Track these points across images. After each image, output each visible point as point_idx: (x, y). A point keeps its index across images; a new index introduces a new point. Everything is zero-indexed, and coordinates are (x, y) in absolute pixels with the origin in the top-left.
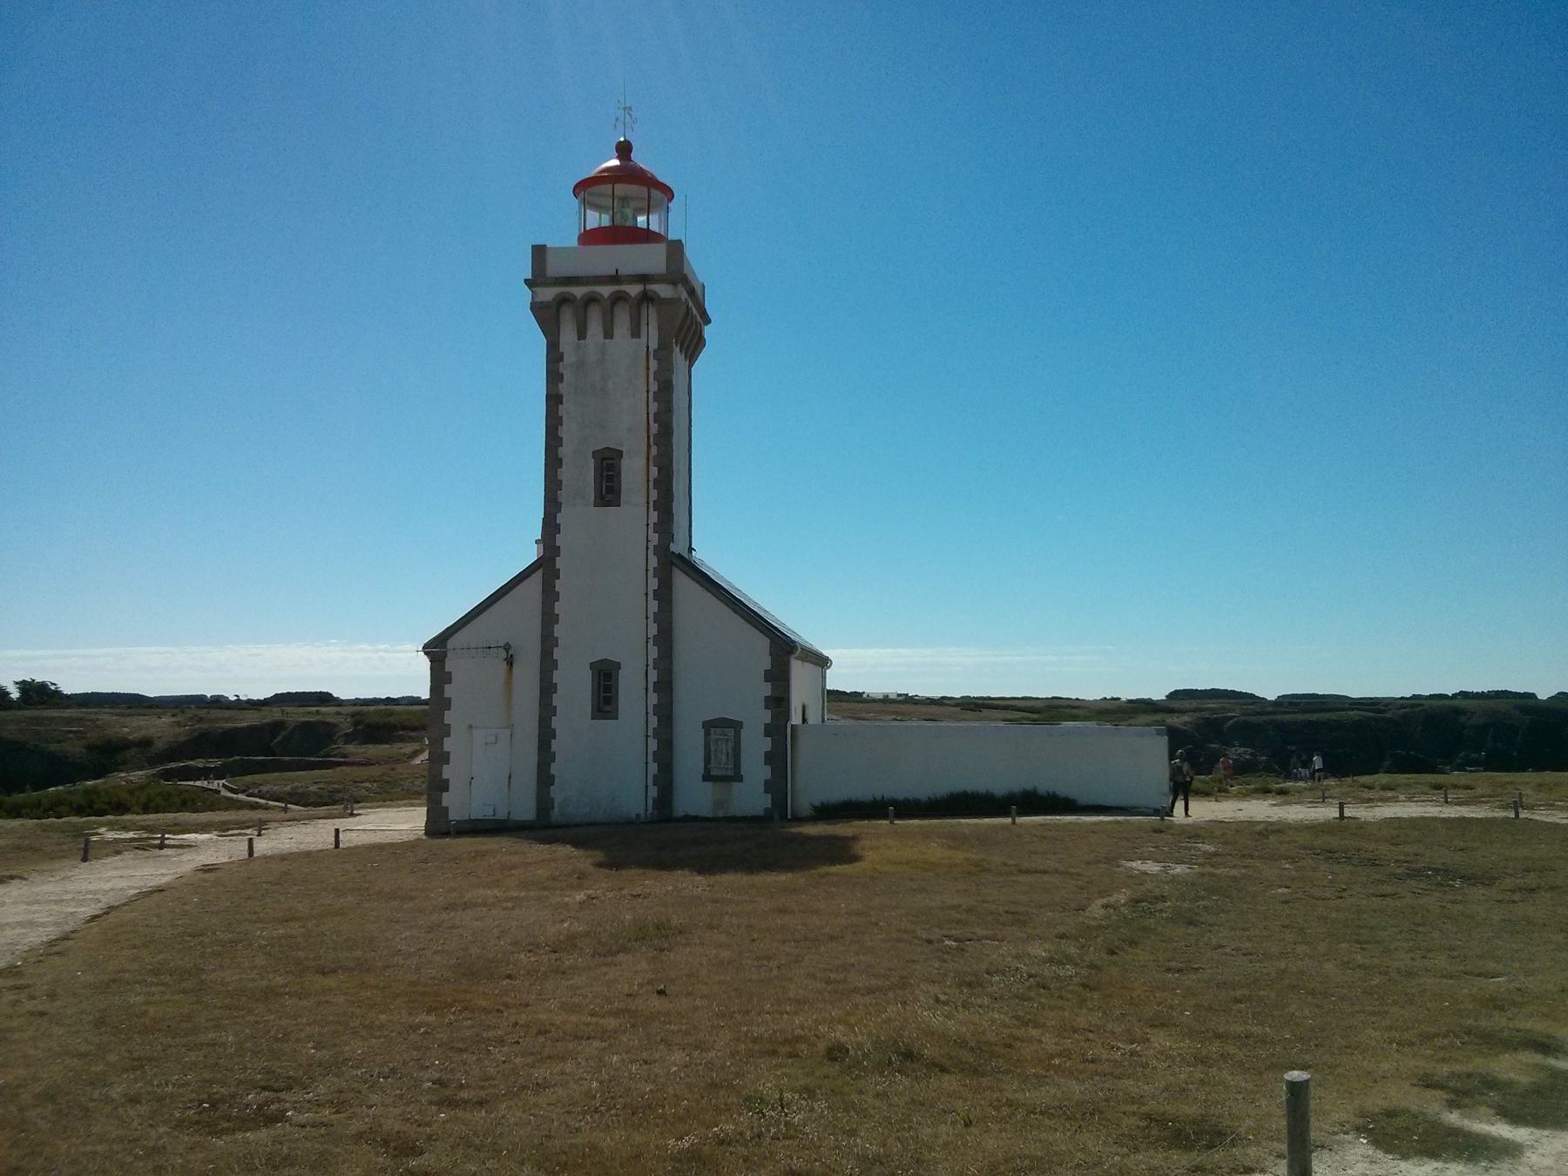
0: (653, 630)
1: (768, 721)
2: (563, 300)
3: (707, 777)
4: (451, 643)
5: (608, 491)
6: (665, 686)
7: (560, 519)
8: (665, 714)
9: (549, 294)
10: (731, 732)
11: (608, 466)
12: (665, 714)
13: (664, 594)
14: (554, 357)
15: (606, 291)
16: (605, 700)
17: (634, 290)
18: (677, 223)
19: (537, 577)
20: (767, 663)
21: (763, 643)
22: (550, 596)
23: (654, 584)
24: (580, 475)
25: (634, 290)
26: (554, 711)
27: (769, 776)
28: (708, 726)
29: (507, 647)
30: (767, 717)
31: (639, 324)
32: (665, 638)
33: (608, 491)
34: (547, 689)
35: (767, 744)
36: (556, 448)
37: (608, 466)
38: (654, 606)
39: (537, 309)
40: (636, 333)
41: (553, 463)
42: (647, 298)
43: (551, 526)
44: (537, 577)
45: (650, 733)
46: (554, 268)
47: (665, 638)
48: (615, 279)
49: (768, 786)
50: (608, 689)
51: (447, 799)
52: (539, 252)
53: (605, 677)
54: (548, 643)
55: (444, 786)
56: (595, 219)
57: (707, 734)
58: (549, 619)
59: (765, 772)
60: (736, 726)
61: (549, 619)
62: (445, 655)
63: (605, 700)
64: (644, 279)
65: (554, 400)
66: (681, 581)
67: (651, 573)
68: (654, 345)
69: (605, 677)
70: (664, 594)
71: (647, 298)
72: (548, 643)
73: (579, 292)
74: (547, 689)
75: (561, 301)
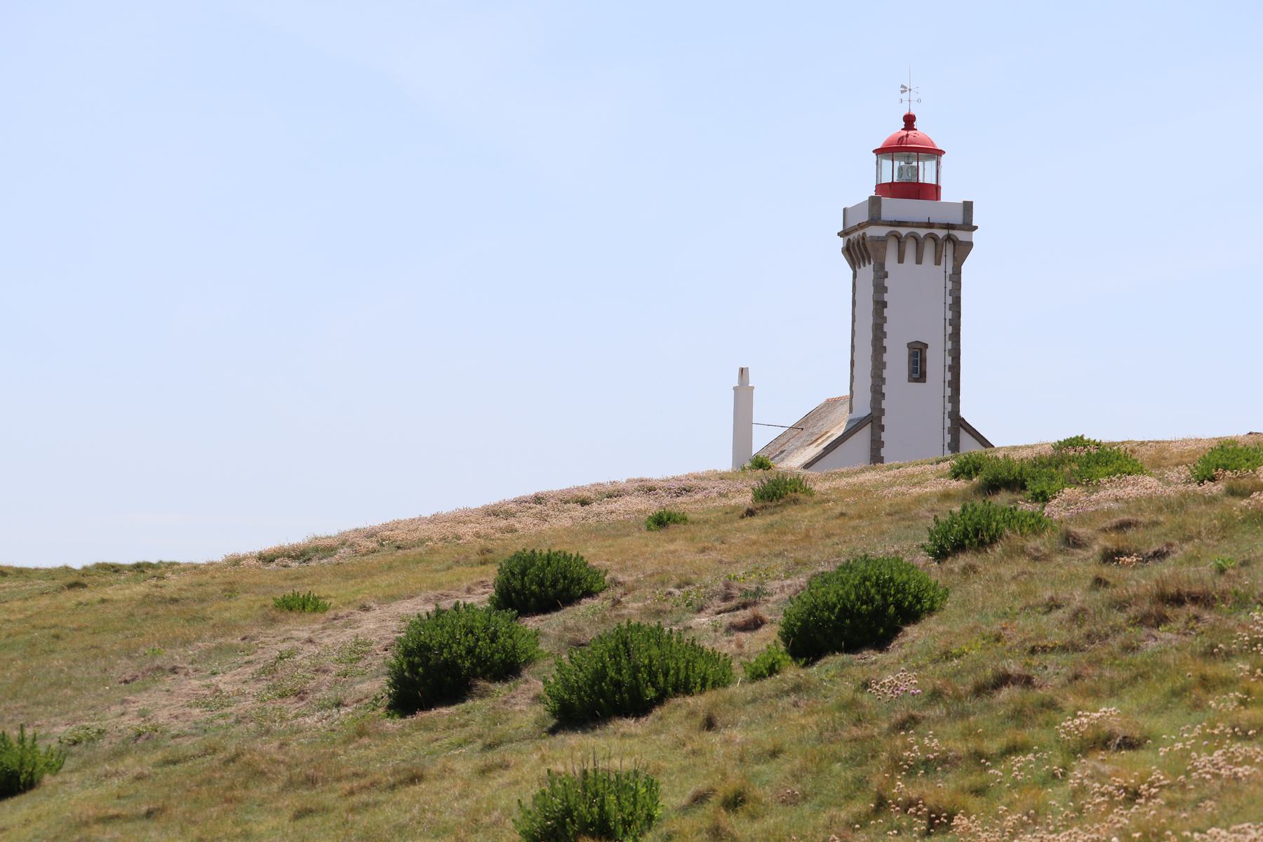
14: (855, 276)
23: (948, 438)
24: (936, 362)
25: (941, 233)
40: (938, 263)
42: (949, 238)
43: (877, 394)
48: (930, 225)
64: (949, 226)
66: (964, 435)
68: (950, 271)
71: (949, 238)
73: (904, 231)
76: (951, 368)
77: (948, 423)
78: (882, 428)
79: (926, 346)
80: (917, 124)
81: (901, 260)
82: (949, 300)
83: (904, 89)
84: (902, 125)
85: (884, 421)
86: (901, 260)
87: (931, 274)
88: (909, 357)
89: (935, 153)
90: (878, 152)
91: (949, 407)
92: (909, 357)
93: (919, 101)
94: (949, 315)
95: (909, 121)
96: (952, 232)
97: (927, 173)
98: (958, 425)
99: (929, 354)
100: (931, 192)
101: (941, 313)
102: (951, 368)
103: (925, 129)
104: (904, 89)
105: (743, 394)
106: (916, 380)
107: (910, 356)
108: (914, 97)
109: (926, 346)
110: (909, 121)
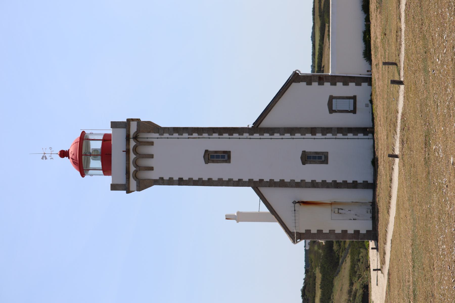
0: (288, 135)
1: (329, 83)
2: (135, 177)
3: (354, 111)
4: (292, 229)
5: (224, 157)
6: (313, 131)
7: (236, 179)
8: (325, 131)
9: (133, 183)
10: (334, 101)
11: (211, 157)
12: (325, 131)
13: (272, 131)
14: (161, 182)
15: (132, 156)
16: (321, 158)
17: (133, 143)
18: (99, 127)
19: (262, 190)
20: (304, 84)
21: (294, 85)
22: (272, 184)
23: (266, 135)
24: (217, 170)
25: (133, 143)
26: (271, 181)
27: (354, 84)
28: (331, 111)
29: (295, 203)
30: (327, 84)
31: (144, 142)
32: (292, 131)
33: (224, 157)
34: (314, 185)
35: (340, 84)
36: (203, 181)
37: (211, 157)
38: (277, 135)
39: (140, 188)
40: (152, 144)
41: (210, 183)
42: (136, 138)
43: (239, 183)
44: (262, 190)
45: (334, 137)
46: (122, 181)
47: (292, 131)
48: (127, 152)
49: (358, 84)
50: (315, 158)
51: (363, 231)
52: (114, 187)
53: (307, 158)
54: (294, 184)
55: (357, 232)
56: (96, 163)
57: (335, 111)
58: (282, 184)
59: (352, 85)
60: (331, 98)
61: (282, 184)
62: (298, 233)
63: (321, 158)
64: (128, 138)
65: (181, 182)
66: (265, 124)
67: (262, 137)
68: (157, 135)
69: (307, 158)
70: (272, 131)
71: (136, 138)
72: (294, 184)
73: (132, 169)
74: (314, 185)
75: (136, 178)
76: (220, 134)
77: (256, 135)
78: (261, 181)
79: (206, 151)
80: (65, 149)
81: (151, 169)
82: (176, 135)
83: (44, 157)
84: (66, 158)
85: (256, 179)
86: (151, 169)
87: (160, 148)
88: (214, 155)
89: (84, 138)
90: (83, 175)
91: (246, 135)
92: (214, 155)
93: (51, 148)
94: (185, 135)
95: (64, 154)
96: (131, 136)
97: (96, 145)
98: (257, 128)
99: (212, 148)
100: (107, 140)
101: (185, 142)
102: (220, 134)
103: (69, 145)
104: (44, 157)
105: (241, 217)
106: (229, 157)
107: (213, 162)
108: (48, 151)
109: (206, 151)
110: (64, 154)
